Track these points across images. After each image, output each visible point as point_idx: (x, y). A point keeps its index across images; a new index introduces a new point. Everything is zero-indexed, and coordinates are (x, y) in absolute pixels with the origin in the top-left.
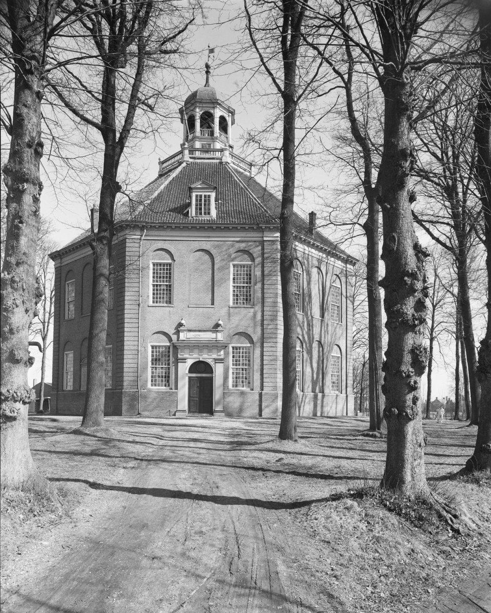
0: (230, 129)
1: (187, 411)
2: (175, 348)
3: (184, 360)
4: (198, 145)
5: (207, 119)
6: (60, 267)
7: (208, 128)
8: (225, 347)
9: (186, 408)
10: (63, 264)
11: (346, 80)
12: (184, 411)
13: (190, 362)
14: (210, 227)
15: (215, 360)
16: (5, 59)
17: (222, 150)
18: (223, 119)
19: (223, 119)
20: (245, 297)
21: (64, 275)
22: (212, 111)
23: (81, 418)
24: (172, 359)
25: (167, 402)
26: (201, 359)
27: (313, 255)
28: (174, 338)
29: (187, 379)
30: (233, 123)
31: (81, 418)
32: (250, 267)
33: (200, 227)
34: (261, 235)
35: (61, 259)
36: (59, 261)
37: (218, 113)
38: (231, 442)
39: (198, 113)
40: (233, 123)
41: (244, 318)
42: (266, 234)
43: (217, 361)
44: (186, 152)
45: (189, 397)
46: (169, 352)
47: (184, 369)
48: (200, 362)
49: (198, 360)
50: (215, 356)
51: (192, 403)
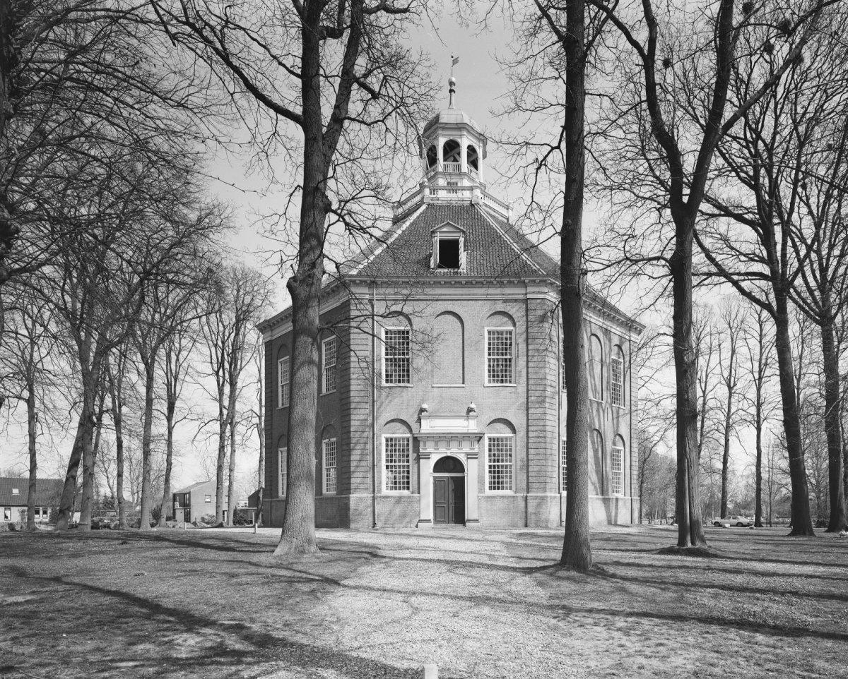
0: (481, 163)
1: (432, 521)
2: (416, 440)
3: (427, 457)
4: (442, 182)
5: (452, 148)
6: (270, 341)
7: (453, 161)
8: (479, 438)
9: (431, 517)
10: (274, 337)
11: (646, 52)
12: (429, 521)
13: (435, 458)
14: (459, 282)
15: (467, 454)
16: (172, 22)
17: (471, 189)
18: (471, 150)
19: (471, 150)
20: (501, 372)
21: (275, 352)
22: (459, 140)
23: (281, 530)
24: (412, 456)
25: (408, 515)
26: (449, 454)
27: (592, 320)
28: (414, 426)
29: (431, 480)
30: (484, 157)
31: (281, 530)
32: (511, 333)
33: (445, 282)
34: (524, 292)
35: (272, 330)
36: (270, 333)
37: (465, 142)
38: (528, 568)
39: (441, 142)
40: (484, 157)
41: (508, 400)
42: (530, 289)
43: (470, 456)
44: (427, 191)
45: (435, 503)
46: (408, 445)
47: (428, 466)
48: (448, 458)
49: (445, 455)
50: (467, 450)
51: (438, 512)
